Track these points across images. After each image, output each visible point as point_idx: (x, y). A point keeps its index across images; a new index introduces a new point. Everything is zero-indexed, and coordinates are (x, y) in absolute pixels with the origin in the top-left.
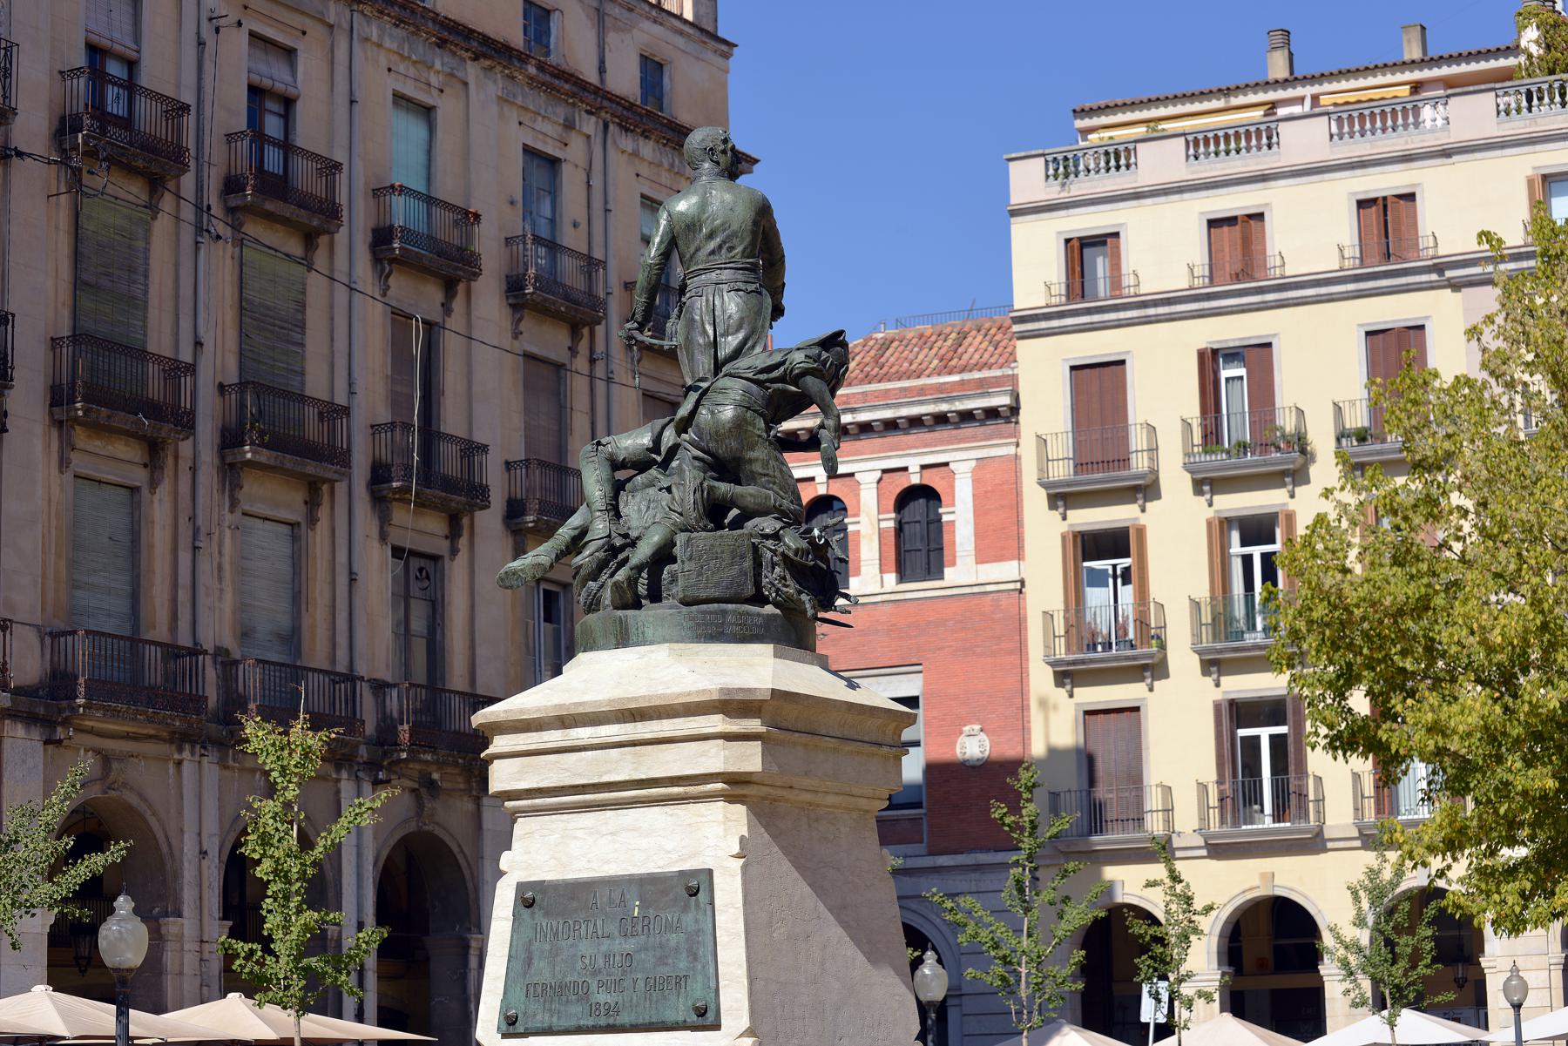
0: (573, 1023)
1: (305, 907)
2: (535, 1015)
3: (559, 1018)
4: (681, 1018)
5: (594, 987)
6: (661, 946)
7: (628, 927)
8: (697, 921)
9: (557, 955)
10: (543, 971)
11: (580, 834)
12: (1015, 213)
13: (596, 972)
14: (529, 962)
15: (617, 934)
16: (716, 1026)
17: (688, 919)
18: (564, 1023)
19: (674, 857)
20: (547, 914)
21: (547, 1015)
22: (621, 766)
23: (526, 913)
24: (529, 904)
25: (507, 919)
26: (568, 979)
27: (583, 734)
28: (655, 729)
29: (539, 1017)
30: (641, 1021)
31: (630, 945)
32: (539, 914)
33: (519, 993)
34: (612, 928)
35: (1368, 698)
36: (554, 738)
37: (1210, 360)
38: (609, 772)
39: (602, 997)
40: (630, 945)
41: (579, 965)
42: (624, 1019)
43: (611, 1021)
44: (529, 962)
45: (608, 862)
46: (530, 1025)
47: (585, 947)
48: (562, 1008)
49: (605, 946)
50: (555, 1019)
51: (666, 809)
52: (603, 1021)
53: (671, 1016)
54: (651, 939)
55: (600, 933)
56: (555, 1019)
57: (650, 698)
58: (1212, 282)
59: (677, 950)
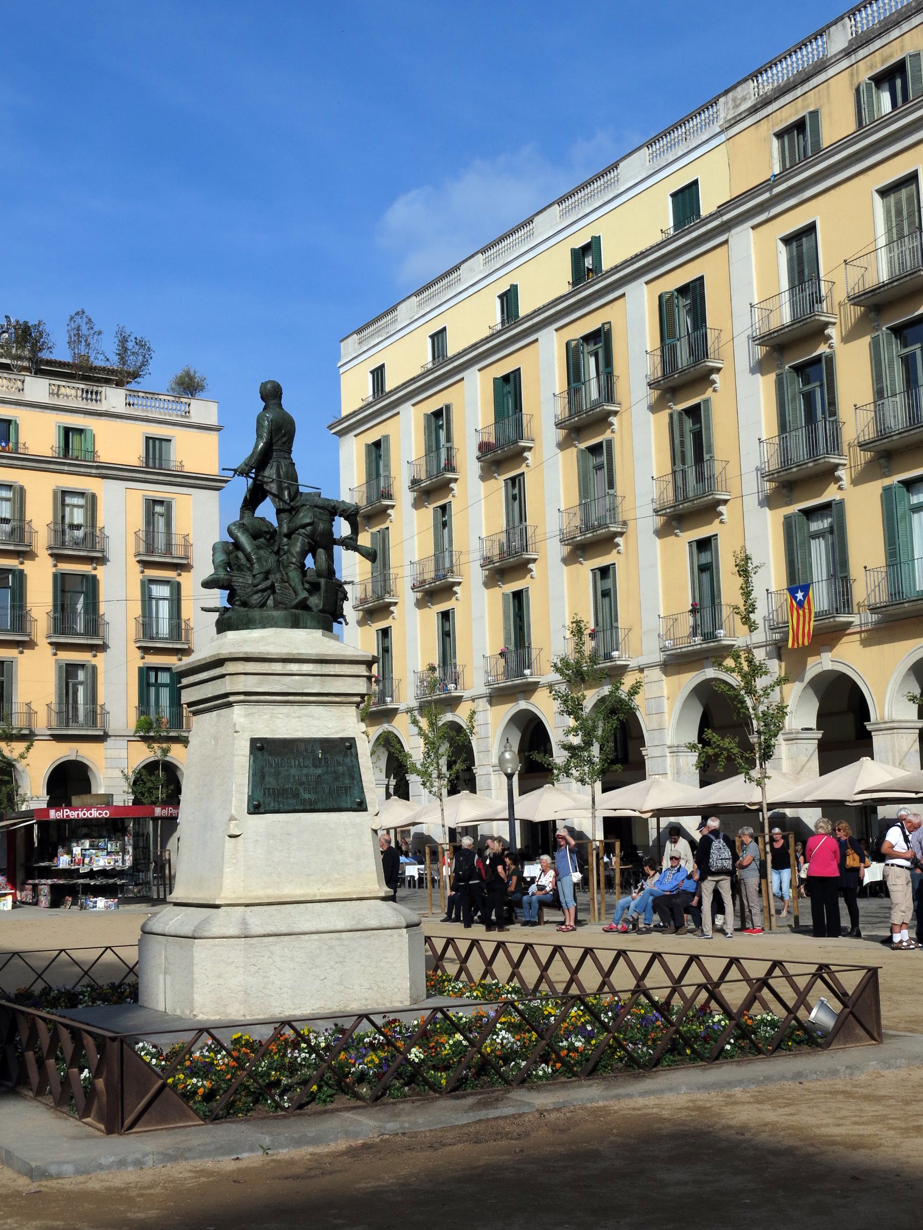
0: (291, 808)
1: (710, 751)
2: (269, 804)
3: (283, 805)
4: (349, 806)
5: (302, 790)
6: (335, 772)
7: (316, 763)
8: (352, 761)
9: (279, 775)
10: (271, 781)
11: (280, 716)
12: (217, 429)
13: (302, 784)
14: (263, 777)
15: (311, 765)
16: (366, 810)
17: (348, 760)
18: (286, 808)
19: (333, 731)
20: (271, 754)
21: (276, 804)
22: (315, 686)
23: (259, 754)
24: (261, 749)
25: (244, 756)
26: (287, 786)
27: (294, 667)
28: (273, 668)
29: (272, 805)
30: (328, 807)
31: (319, 771)
32: (266, 755)
33: (259, 795)
34: (309, 763)
35: (623, 681)
36: (278, 667)
37: (151, 503)
38: (308, 688)
39: (307, 796)
40: (319, 771)
41: (292, 780)
42: (320, 806)
43: (313, 807)
44: (263, 777)
45: (298, 731)
46: (267, 808)
47: (293, 771)
48: (285, 801)
49: (305, 771)
50: (281, 806)
51: (326, 708)
52: (308, 807)
53: (344, 805)
54: (329, 769)
55: (302, 765)
56: (281, 806)
57: (338, 655)
58: (147, 466)
59: (343, 774)
